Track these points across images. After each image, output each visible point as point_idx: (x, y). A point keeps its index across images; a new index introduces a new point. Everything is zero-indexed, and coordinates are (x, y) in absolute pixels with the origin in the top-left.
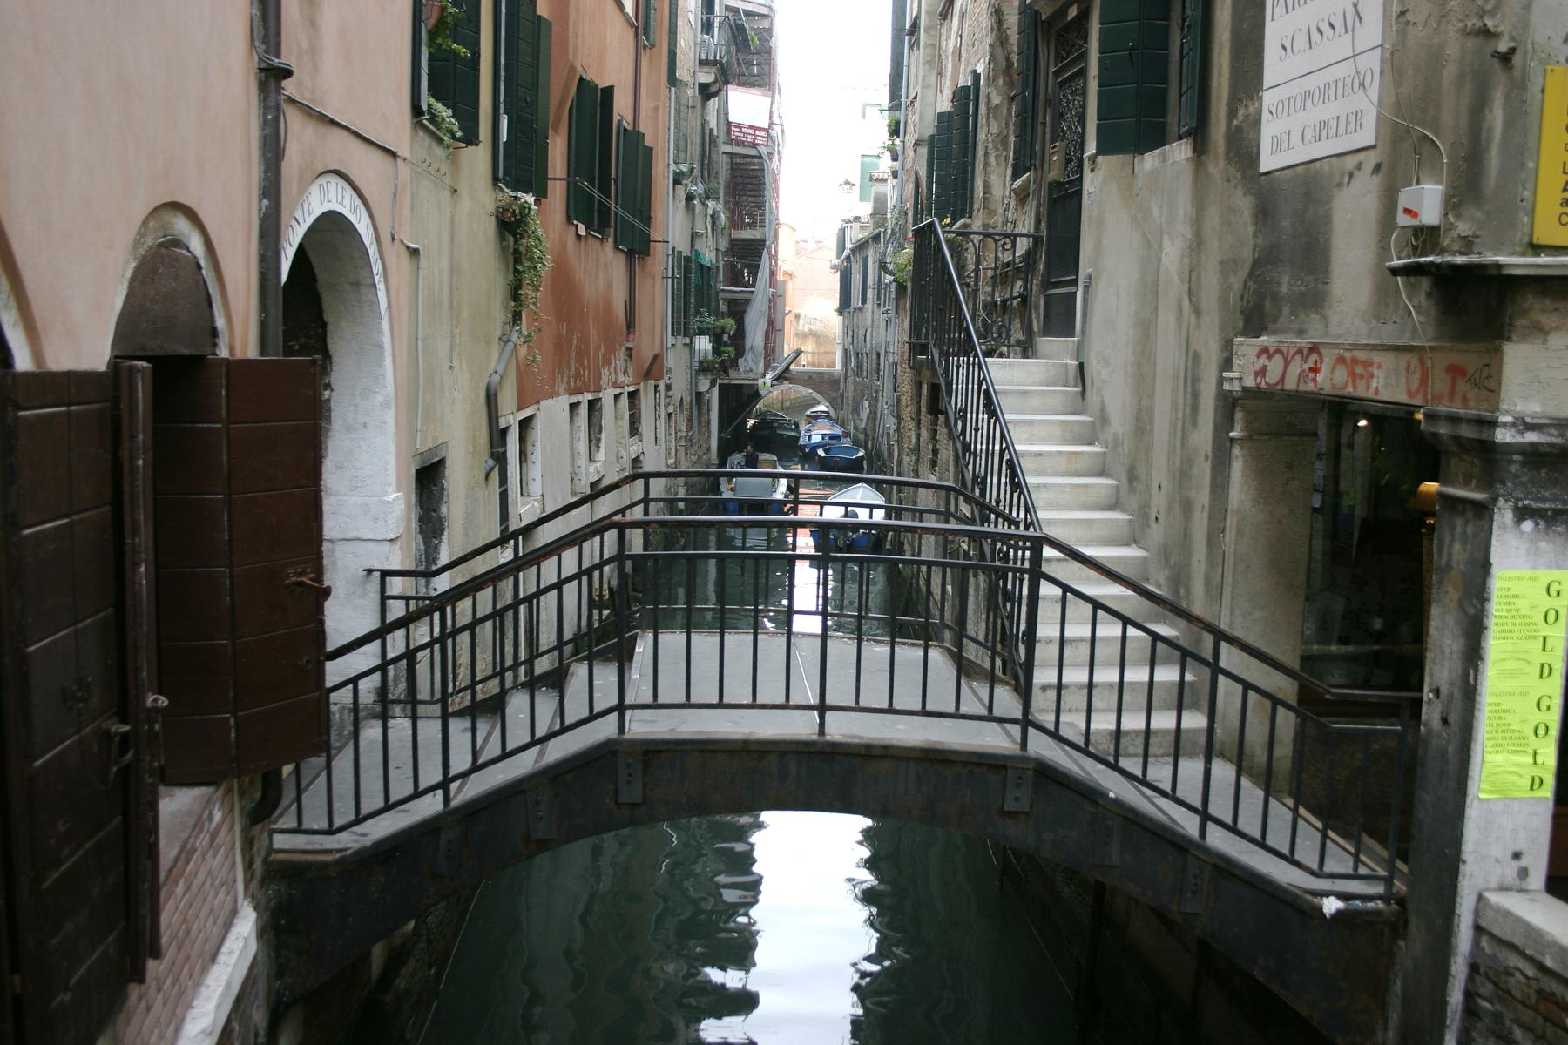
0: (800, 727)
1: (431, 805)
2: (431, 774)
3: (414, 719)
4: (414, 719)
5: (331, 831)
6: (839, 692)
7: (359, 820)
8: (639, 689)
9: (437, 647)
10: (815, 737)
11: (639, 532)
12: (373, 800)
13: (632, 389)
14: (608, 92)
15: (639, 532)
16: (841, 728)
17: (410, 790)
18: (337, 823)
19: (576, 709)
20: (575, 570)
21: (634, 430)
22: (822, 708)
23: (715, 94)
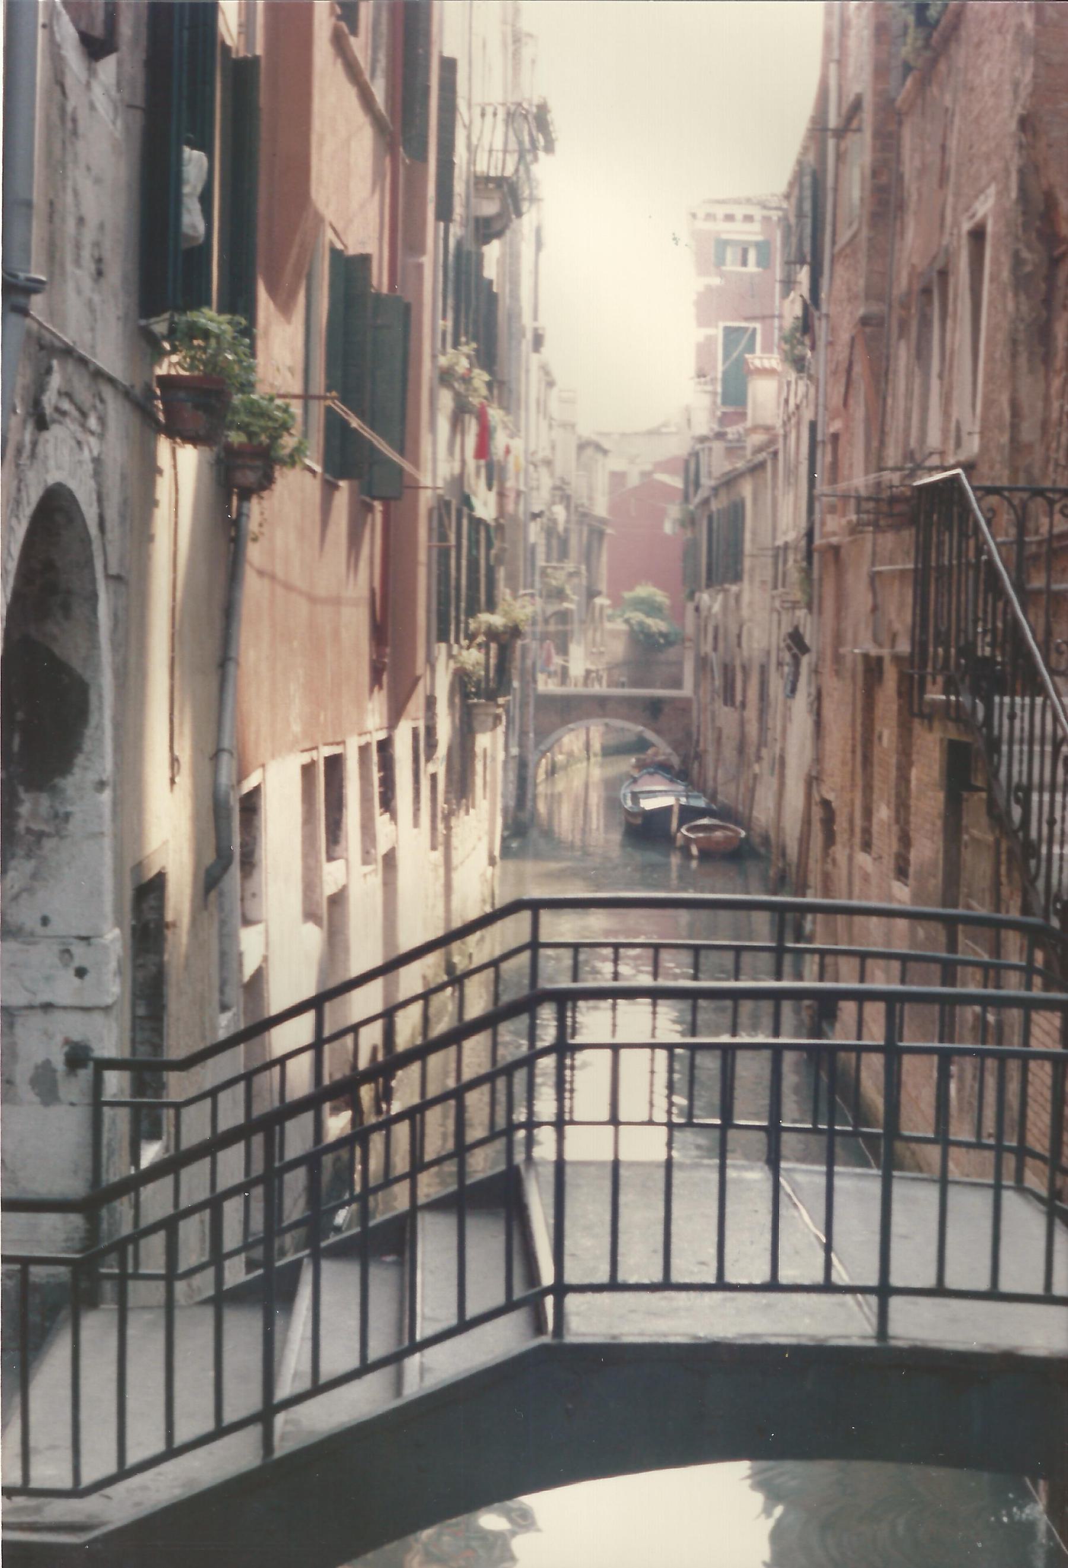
0: (847, 1323)
1: (236, 1455)
2: (243, 1400)
3: (773, 1161)
4: (773, 1161)
5: (77, 1492)
6: (912, 1267)
7: (124, 1473)
8: (587, 1260)
9: (258, 1191)
10: (872, 1343)
11: (881, 1006)
12: (146, 1440)
13: (382, 735)
14: (365, 260)
15: (881, 1006)
16: (917, 1324)
17: (110, 1467)
18: (88, 1477)
19: (434, 1309)
20: (485, 1068)
21: (388, 802)
22: (884, 1291)
23: (499, 234)
